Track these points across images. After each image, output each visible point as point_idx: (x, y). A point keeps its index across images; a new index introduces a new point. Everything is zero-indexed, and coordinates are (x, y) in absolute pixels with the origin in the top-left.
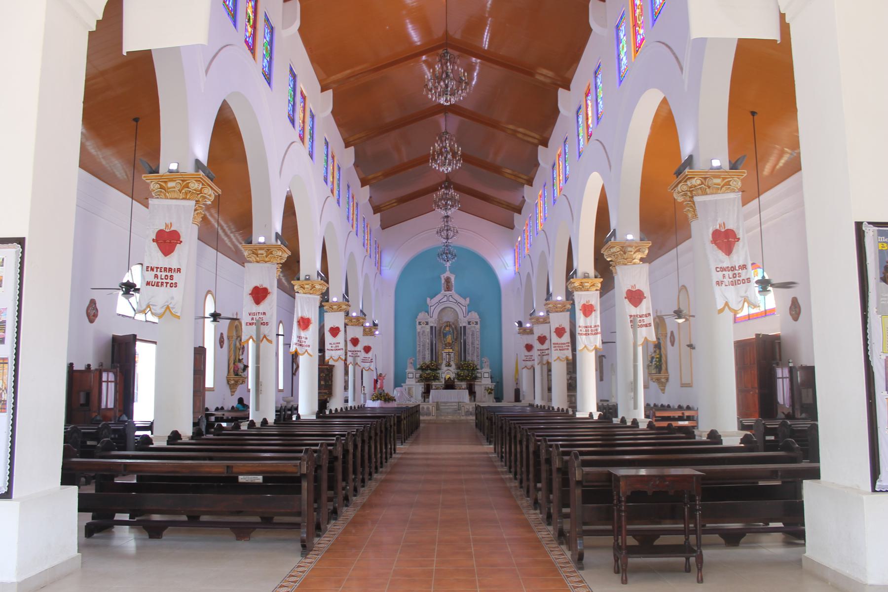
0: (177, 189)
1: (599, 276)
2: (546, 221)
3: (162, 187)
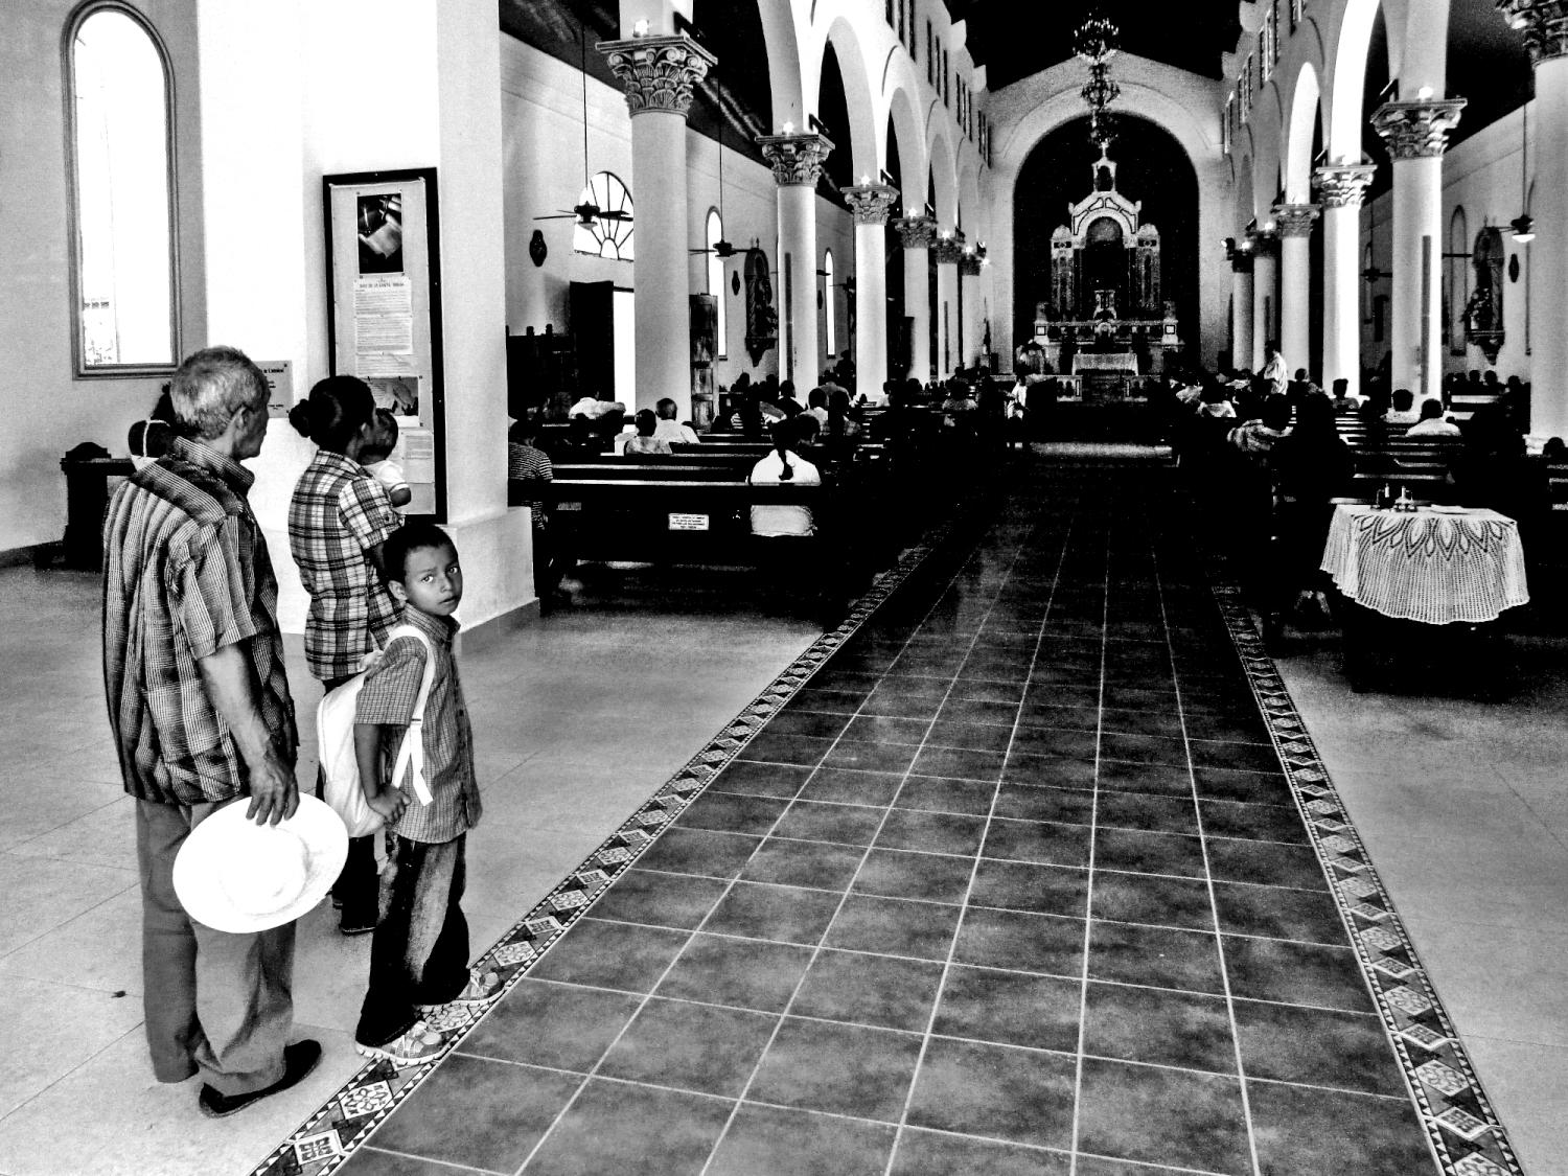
0: (648, 63)
1: (1371, 161)
2: (1296, 35)
3: (626, 60)
